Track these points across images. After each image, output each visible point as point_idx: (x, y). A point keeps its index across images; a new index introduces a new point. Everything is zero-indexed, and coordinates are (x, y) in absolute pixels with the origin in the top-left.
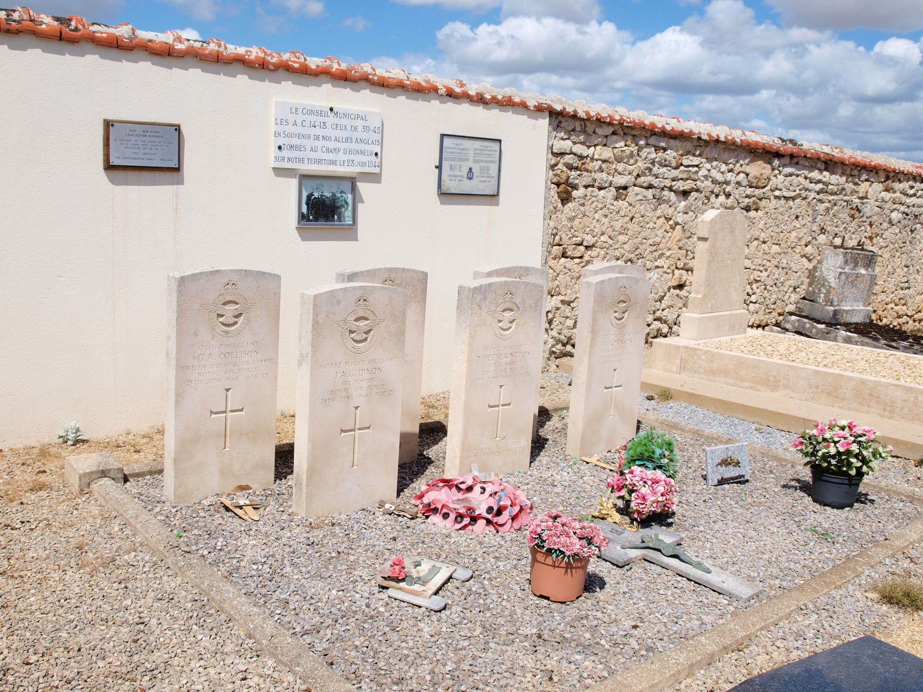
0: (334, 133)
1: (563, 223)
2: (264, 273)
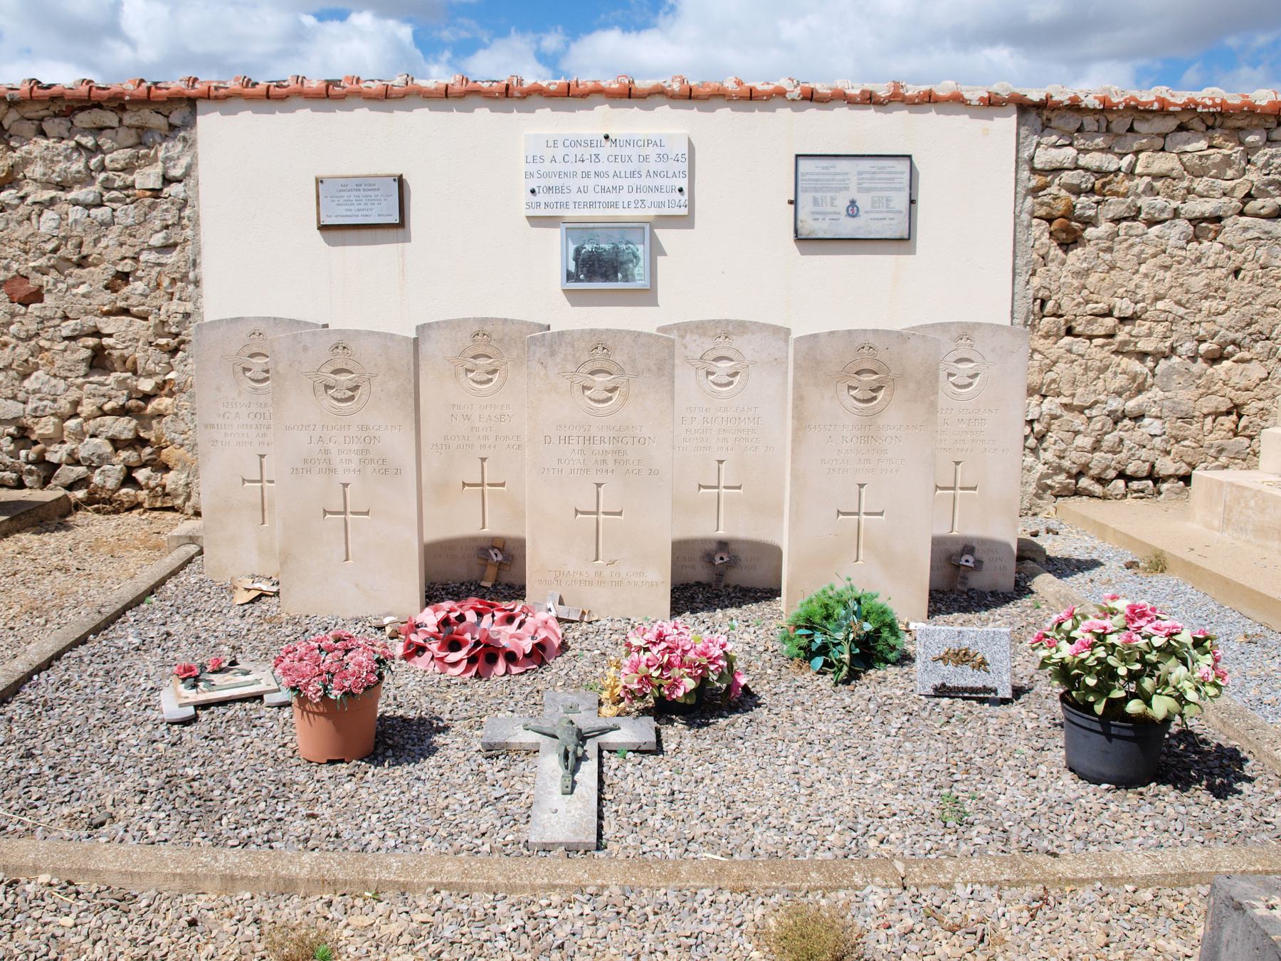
1: (1062, 280)
2: (298, 322)
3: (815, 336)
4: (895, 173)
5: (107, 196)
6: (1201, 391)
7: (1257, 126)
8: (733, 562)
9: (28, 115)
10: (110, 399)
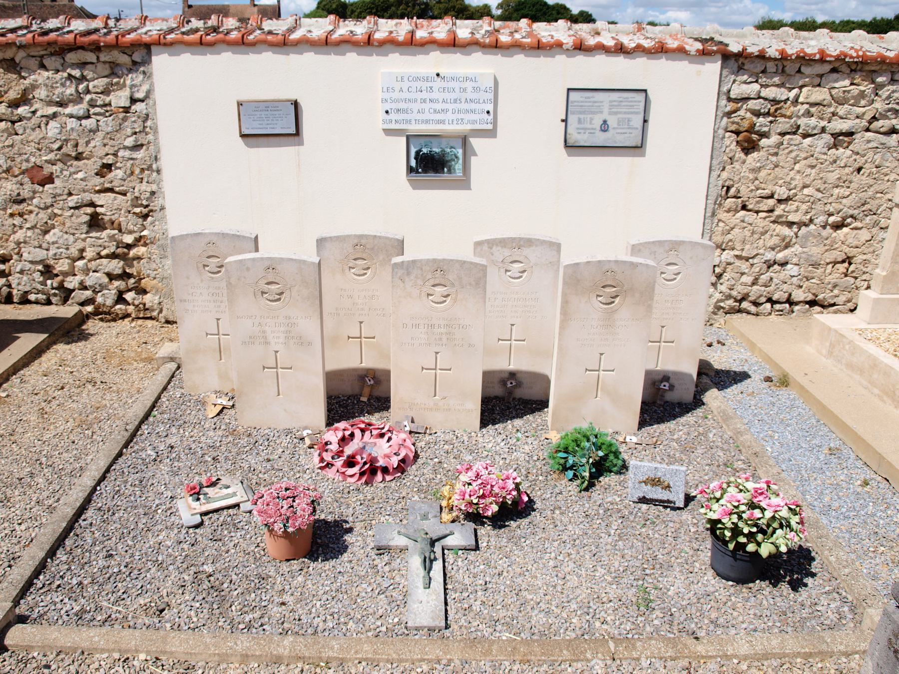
0: (440, 96)
3: (577, 264)
4: (635, 102)
5: (92, 111)
6: (827, 248)
7: (886, 70)
8: (519, 384)
9: (32, 54)
10: (105, 248)
